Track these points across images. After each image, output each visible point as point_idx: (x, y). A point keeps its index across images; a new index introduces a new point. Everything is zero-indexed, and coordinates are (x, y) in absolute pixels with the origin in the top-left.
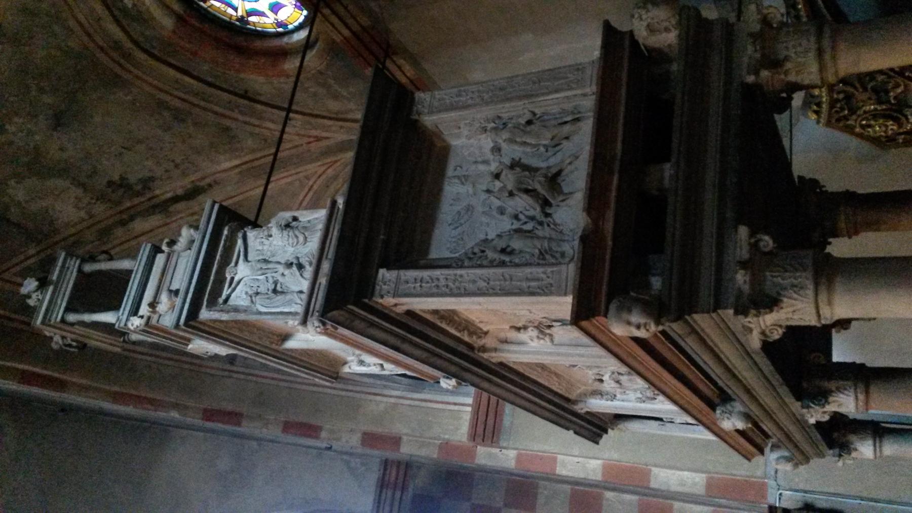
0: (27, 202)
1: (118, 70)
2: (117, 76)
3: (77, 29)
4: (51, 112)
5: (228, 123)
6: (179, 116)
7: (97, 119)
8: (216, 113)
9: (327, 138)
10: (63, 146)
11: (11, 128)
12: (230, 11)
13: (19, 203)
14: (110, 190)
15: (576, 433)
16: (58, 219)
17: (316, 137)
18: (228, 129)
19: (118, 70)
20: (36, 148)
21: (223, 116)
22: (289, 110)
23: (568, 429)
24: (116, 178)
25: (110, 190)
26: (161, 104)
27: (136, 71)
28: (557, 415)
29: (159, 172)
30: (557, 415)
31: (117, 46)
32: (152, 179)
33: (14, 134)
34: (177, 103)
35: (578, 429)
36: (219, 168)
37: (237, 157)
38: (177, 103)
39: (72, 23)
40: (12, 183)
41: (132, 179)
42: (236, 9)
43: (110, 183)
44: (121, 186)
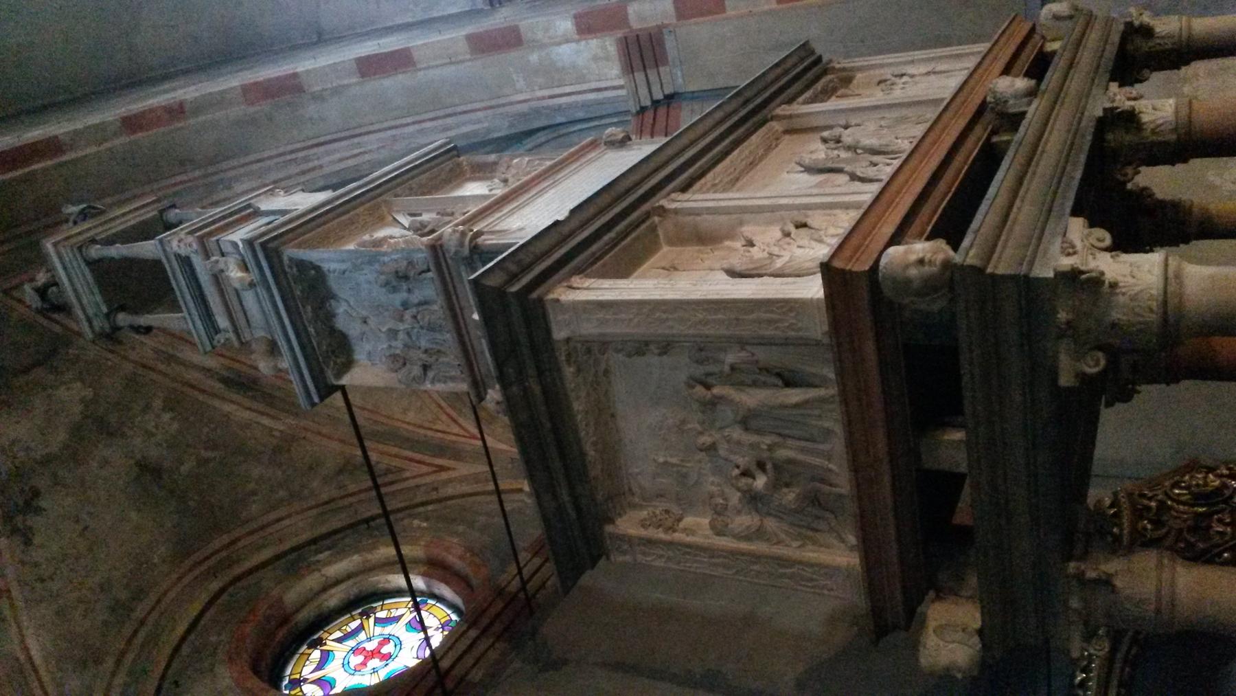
0: (49, 396)
1: (196, 557)
2: (189, 555)
3: (273, 516)
4: (166, 464)
5: (109, 663)
6: (120, 610)
7: (133, 515)
8: (123, 653)
9: (449, 469)
10: (110, 463)
11: (166, 417)
12: (338, 634)
13: (57, 388)
14: (27, 488)
15: (557, 223)
16: (9, 414)
17: (437, 466)
18: (98, 661)
19: (196, 557)
20: (123, 435)
21: (118, 663)
22: (386, 514)
23: (573, 212)
24: (43, 504)
25: (27, 488)
26: (139, 595)
27: (190, 577)
28: (628, 191)
29: (37, 555)
30: (628, 191)
31: (230, 562)
32: (28, 542)
33: (158, 416)
34: (139, 613)
35: (566, 230)
36: (29, 632)
37: (46, 660)
38: (139, 613)
39: (282, 512)
40: (89, 393)
41: (35, 521)
42: (339, 640)
43: (36, 493)
44: (28, 504)
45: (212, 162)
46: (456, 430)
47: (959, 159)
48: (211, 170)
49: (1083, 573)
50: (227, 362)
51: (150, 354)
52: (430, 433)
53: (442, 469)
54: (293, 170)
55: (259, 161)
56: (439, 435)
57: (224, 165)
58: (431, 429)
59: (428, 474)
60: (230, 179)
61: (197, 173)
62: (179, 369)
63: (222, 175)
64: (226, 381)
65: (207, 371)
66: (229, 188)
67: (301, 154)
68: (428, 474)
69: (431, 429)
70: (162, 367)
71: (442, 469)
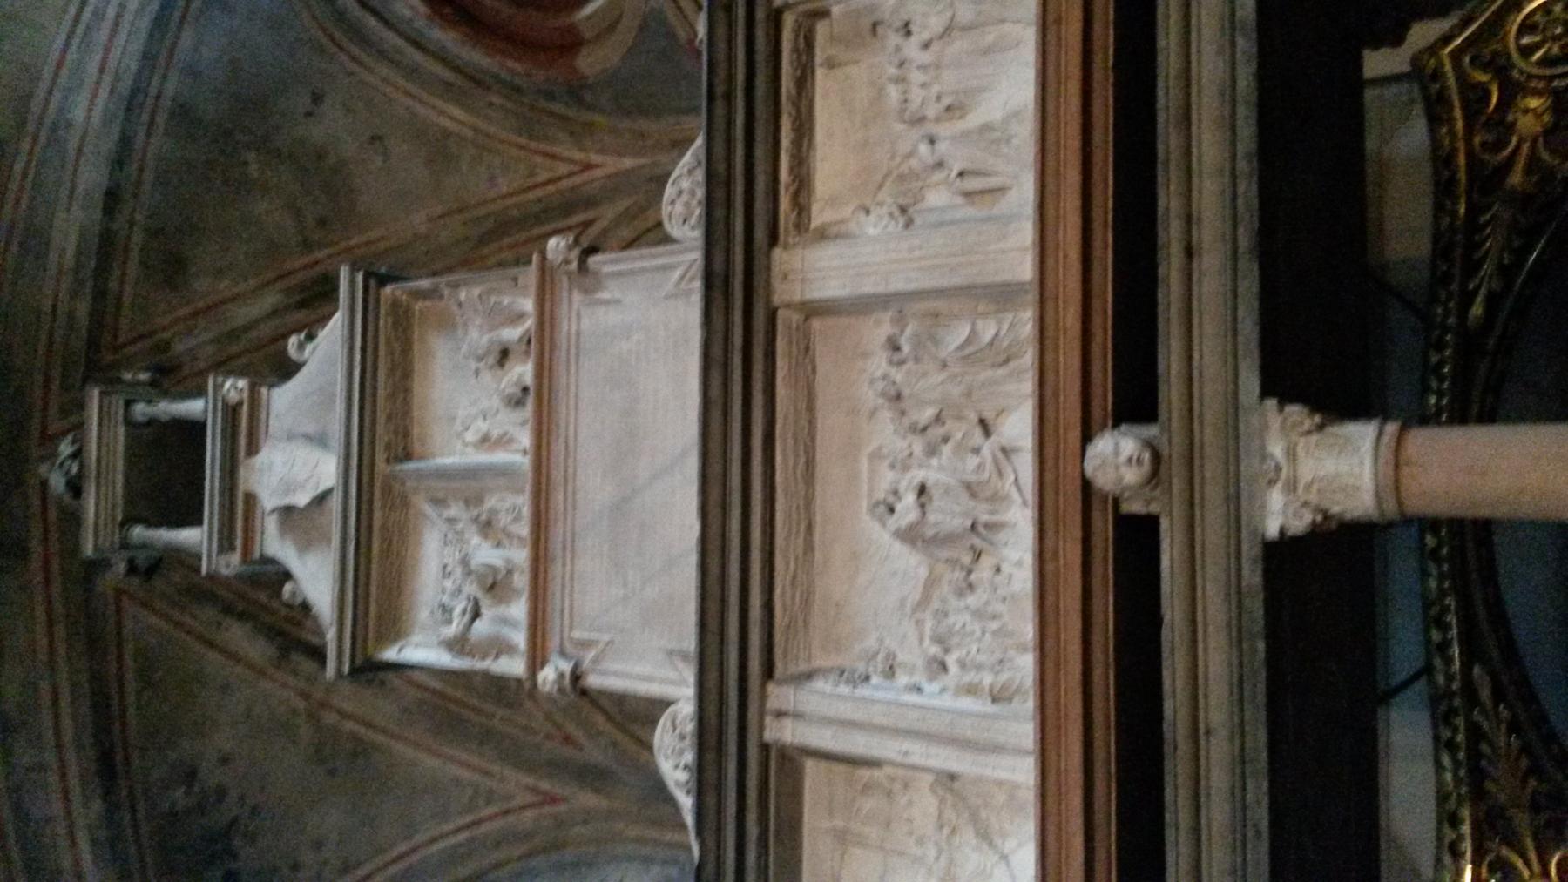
45: (23, 123)
46: (563, 169)
47: (1097, 108)
48: (30, 128)
49: (1457, 714)
50: (279, 285)
51: (210, 349)
52: (539, 193)
53: (587, 224)
54: (102, 36)
55: (60, 65)
56: (551, 188)
57: (35, 107)
58: (536, 186)
59: (570, 175)
60: (61, 110)
61: (25, 145)
62: (254, 334)
63: (48, 121)
64: (302, 304)
65: (274, 313)
66: (69, 125)
67: (87, 15)
68: (570, 175)
69: (536, 186)
70: (234, 349)
71: (587, 224)
